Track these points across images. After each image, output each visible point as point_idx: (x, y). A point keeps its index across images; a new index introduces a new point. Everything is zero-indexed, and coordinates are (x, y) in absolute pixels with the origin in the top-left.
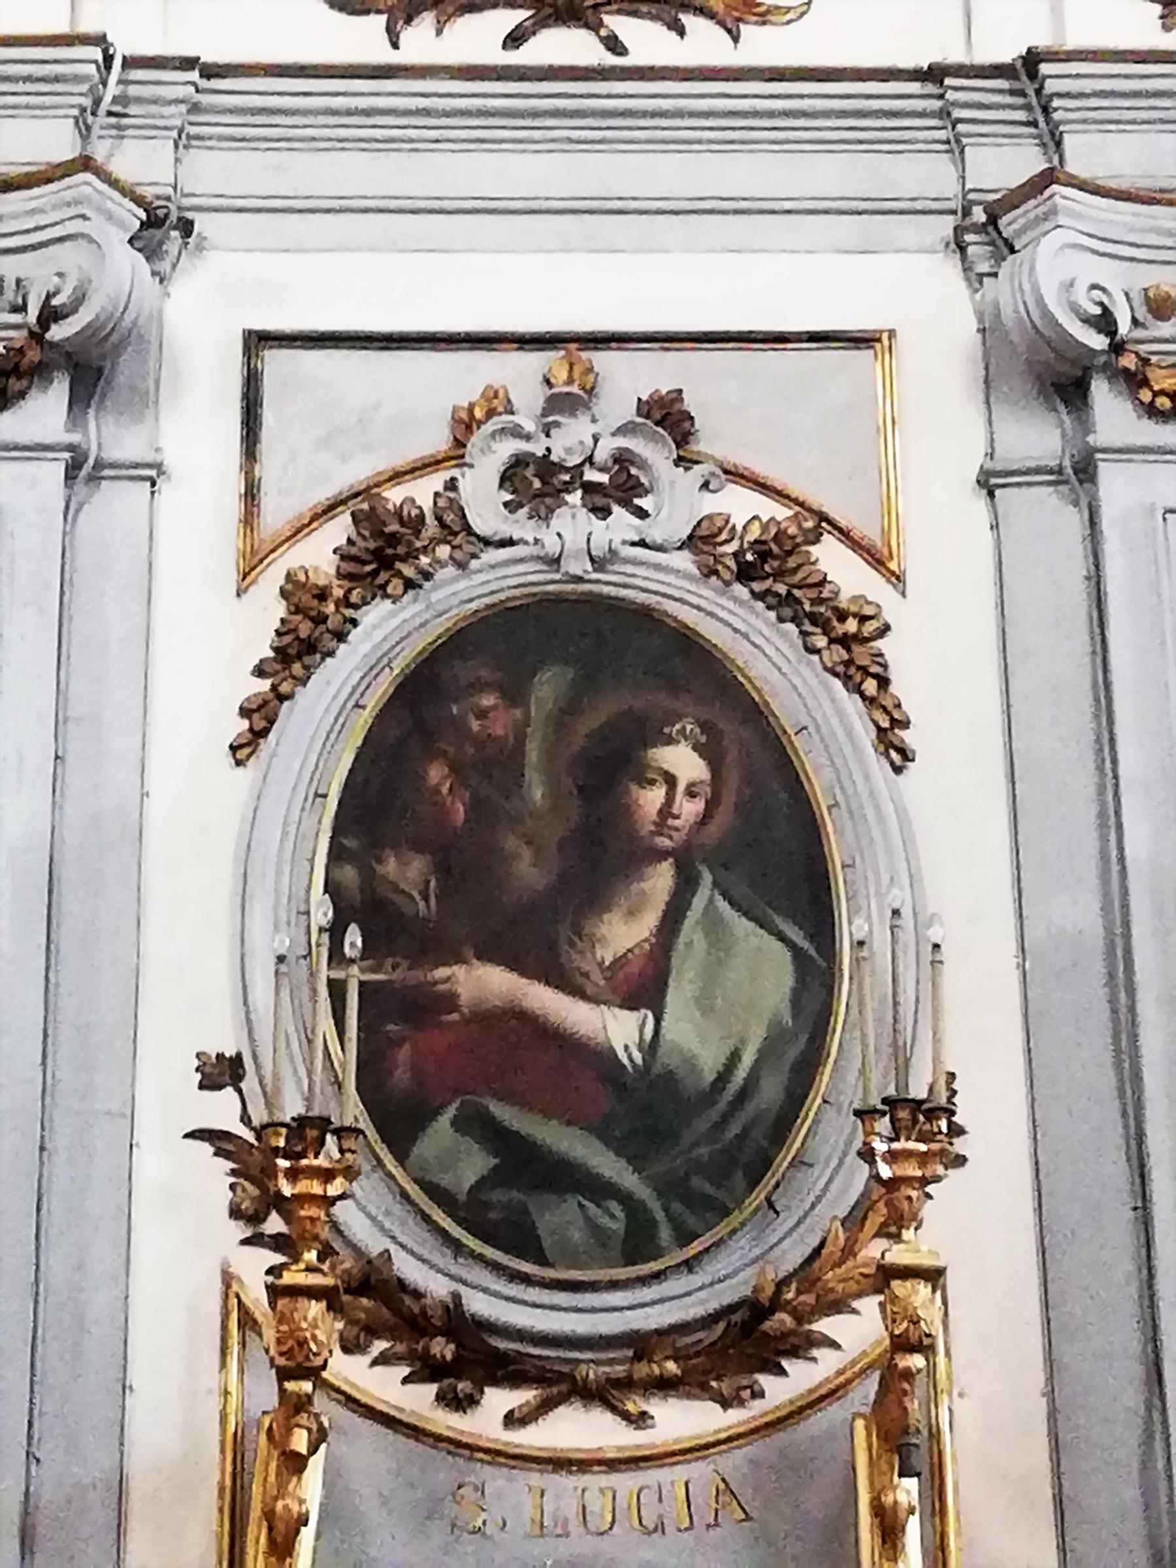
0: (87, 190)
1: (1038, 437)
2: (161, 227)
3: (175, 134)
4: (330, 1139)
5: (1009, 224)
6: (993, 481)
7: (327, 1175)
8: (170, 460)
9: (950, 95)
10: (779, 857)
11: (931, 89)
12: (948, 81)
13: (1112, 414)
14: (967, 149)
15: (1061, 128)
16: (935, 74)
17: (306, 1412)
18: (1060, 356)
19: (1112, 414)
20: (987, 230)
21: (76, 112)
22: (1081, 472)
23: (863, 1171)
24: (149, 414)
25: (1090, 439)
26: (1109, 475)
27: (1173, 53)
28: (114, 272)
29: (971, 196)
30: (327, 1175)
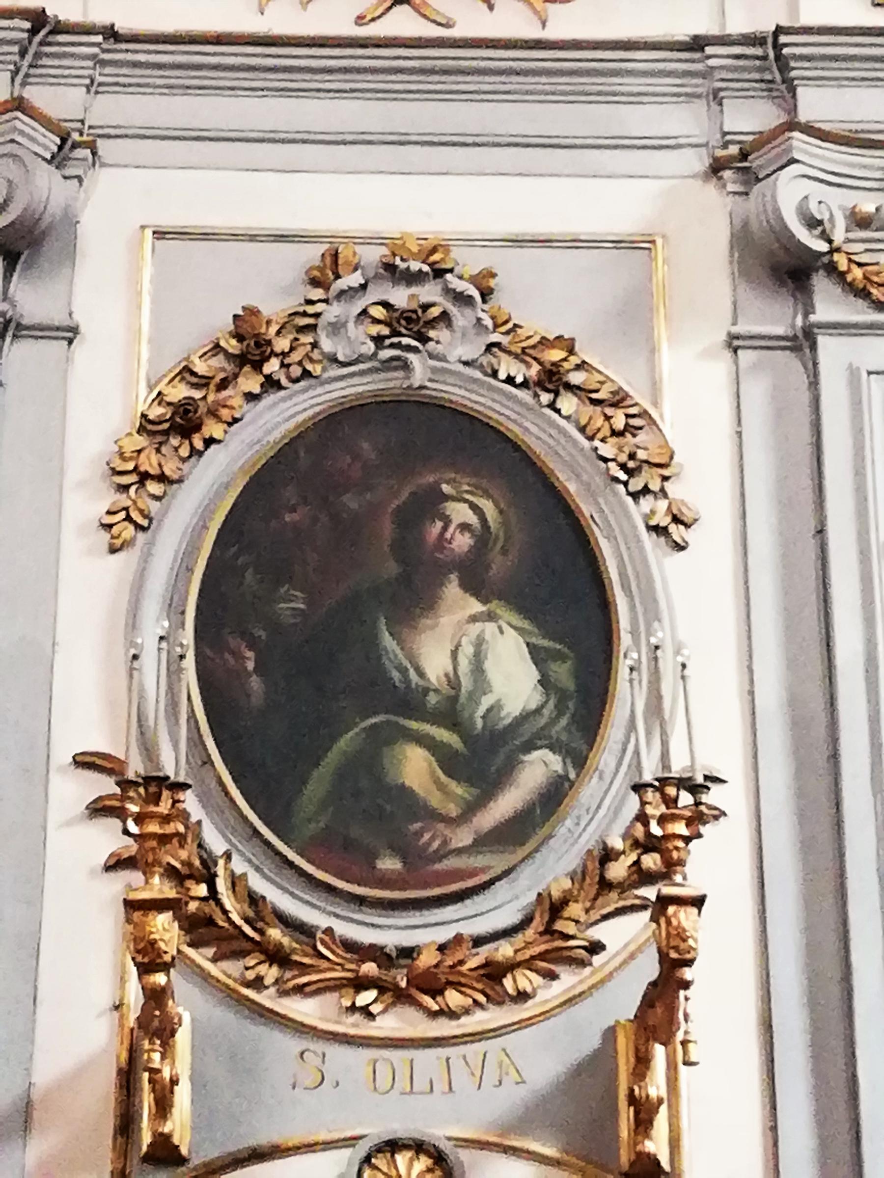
0: (17, 123)
1: (775, 317)
2: (71, 147)
3: (88, 81)
4: (166, 794)
5: (755, 161)
6: (736, 343)
7: (166, 819)
8: (79, 318)
9: (712, 62)
10: (570, 599)
11: (697, 55)
12: (709, 50)
13: (829, 304)
14: (724, 100)
15: (796, 82)
16: (697, 44)
17: (289, 955)
18: (787, 250)
19: (829, 304)
20: (739, 164)
21: (12, 67)
22: (803, 343)
23: (633, 803)
24: (256, 401)
25: (813, 318)
26: (824, 341)
27: (882, 31)
28: (47, 188)
29: (728, 137)
30: (166, 819)
